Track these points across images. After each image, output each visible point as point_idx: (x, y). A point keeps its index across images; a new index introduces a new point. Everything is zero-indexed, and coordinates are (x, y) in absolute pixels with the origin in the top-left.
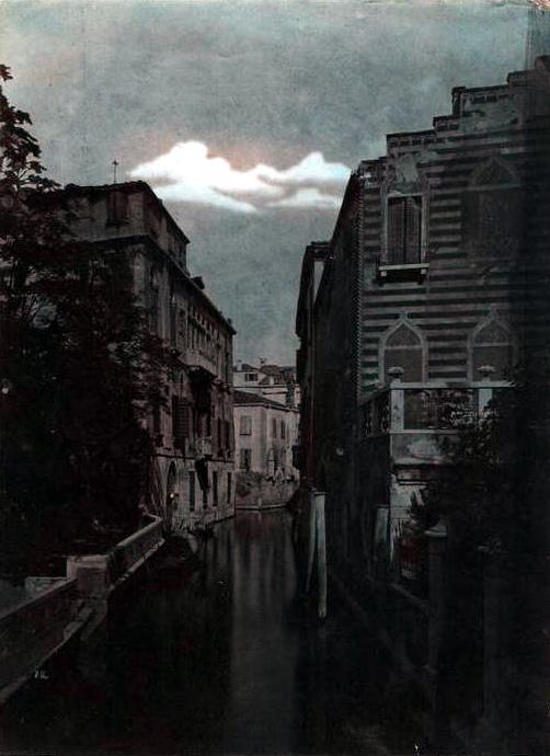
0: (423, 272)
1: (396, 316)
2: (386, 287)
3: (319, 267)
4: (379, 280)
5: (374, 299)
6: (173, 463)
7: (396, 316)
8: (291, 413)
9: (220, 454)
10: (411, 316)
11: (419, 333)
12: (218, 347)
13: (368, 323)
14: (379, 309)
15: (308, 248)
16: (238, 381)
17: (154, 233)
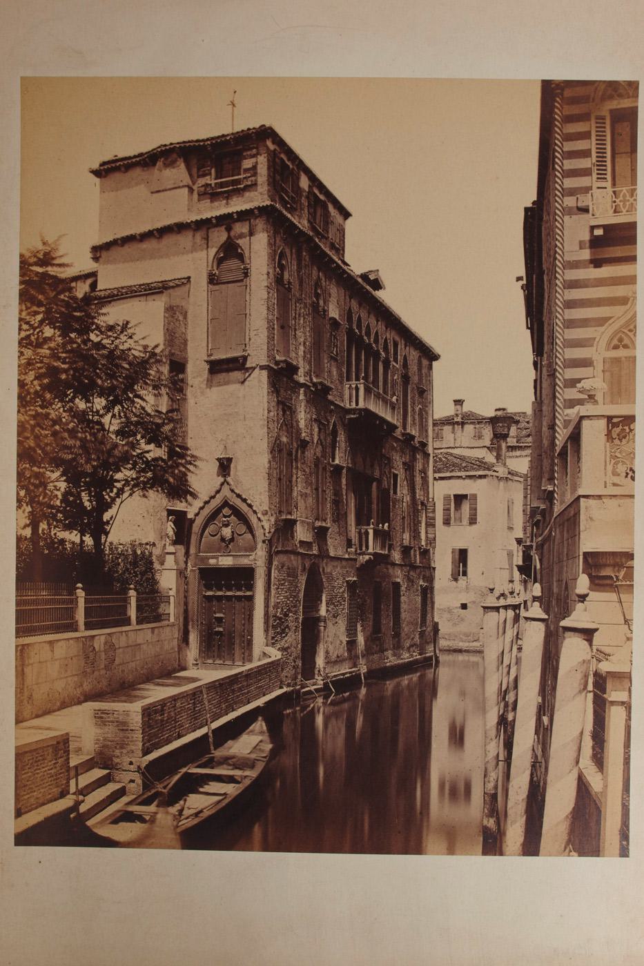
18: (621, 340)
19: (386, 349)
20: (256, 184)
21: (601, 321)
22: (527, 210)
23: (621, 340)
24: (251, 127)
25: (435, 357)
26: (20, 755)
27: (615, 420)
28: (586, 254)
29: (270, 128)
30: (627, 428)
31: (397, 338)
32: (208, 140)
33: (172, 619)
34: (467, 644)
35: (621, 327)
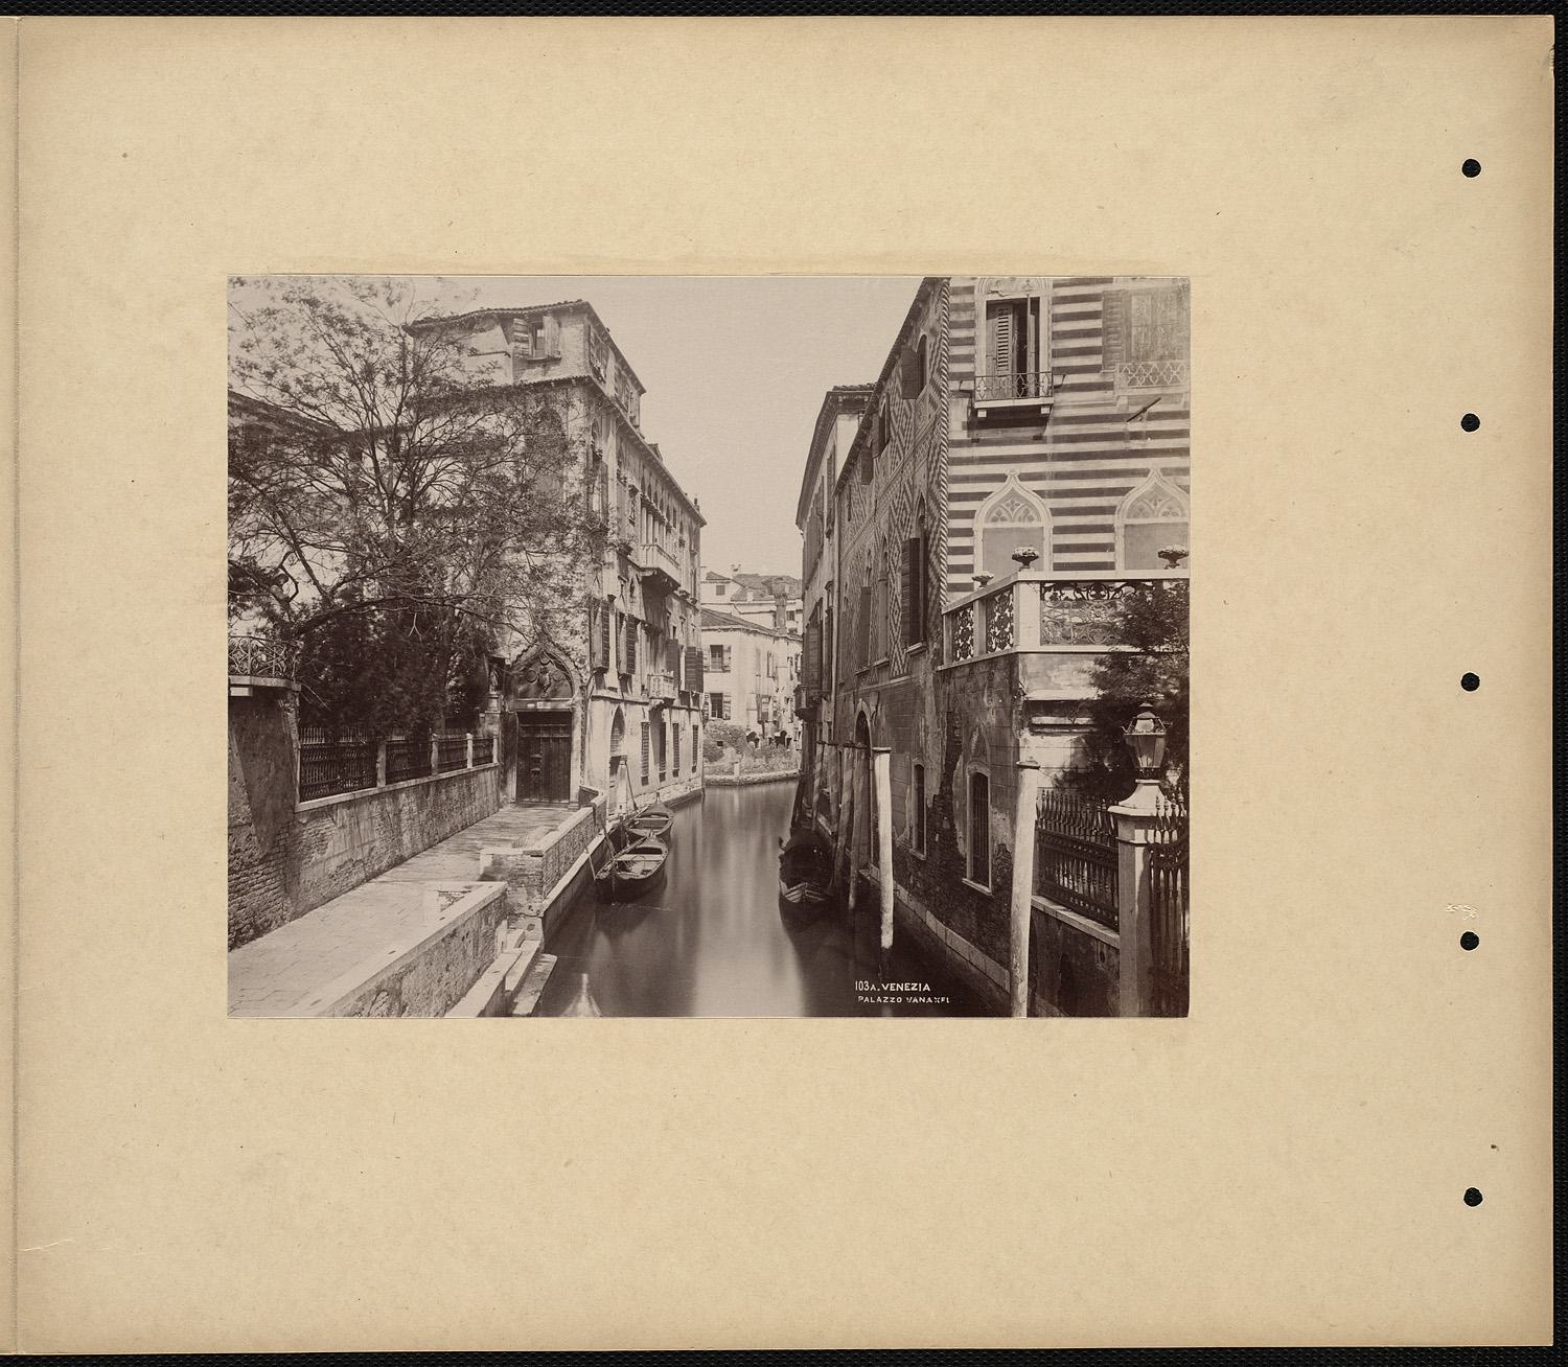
0: (1044, 411)
1: (1002, 478)
2: (985, 434)
3: (847, 429)
4: (974, 424)
5: (965, 452)
6: (619, 709)
7: (1002, 478)
8: (782, 641)
9: (683, 695)
10: (1025, 477)
11: (1035, 500)
12: (682, 543)
13: (956, 488)
14: (1088, 426)
15: (828, 394)
16: (707, 596)
17: (597, 372)
18: (999, 514)
20: (1055, 286)
21: (981, 496)
23: (999, 514)
25: (703, 523)
26: (830, 997)
27: (1047, 585)
28: (963, 436)
29: (587, 304)
30: (1058, 592)
31: (676, 507)
32: (525, 309)
33: (495, 760)
34: (761, 775)
35: (999, 501)
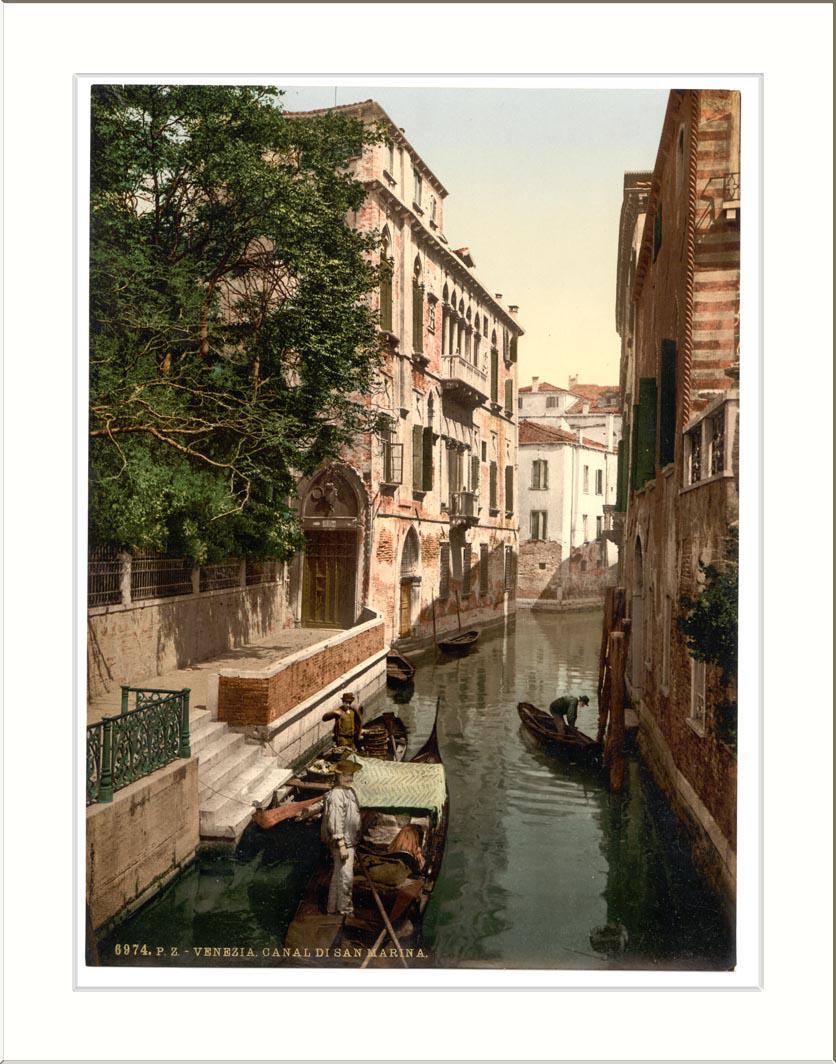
19: (477, 324)
22: (630, 179)
24: (357, 102)
